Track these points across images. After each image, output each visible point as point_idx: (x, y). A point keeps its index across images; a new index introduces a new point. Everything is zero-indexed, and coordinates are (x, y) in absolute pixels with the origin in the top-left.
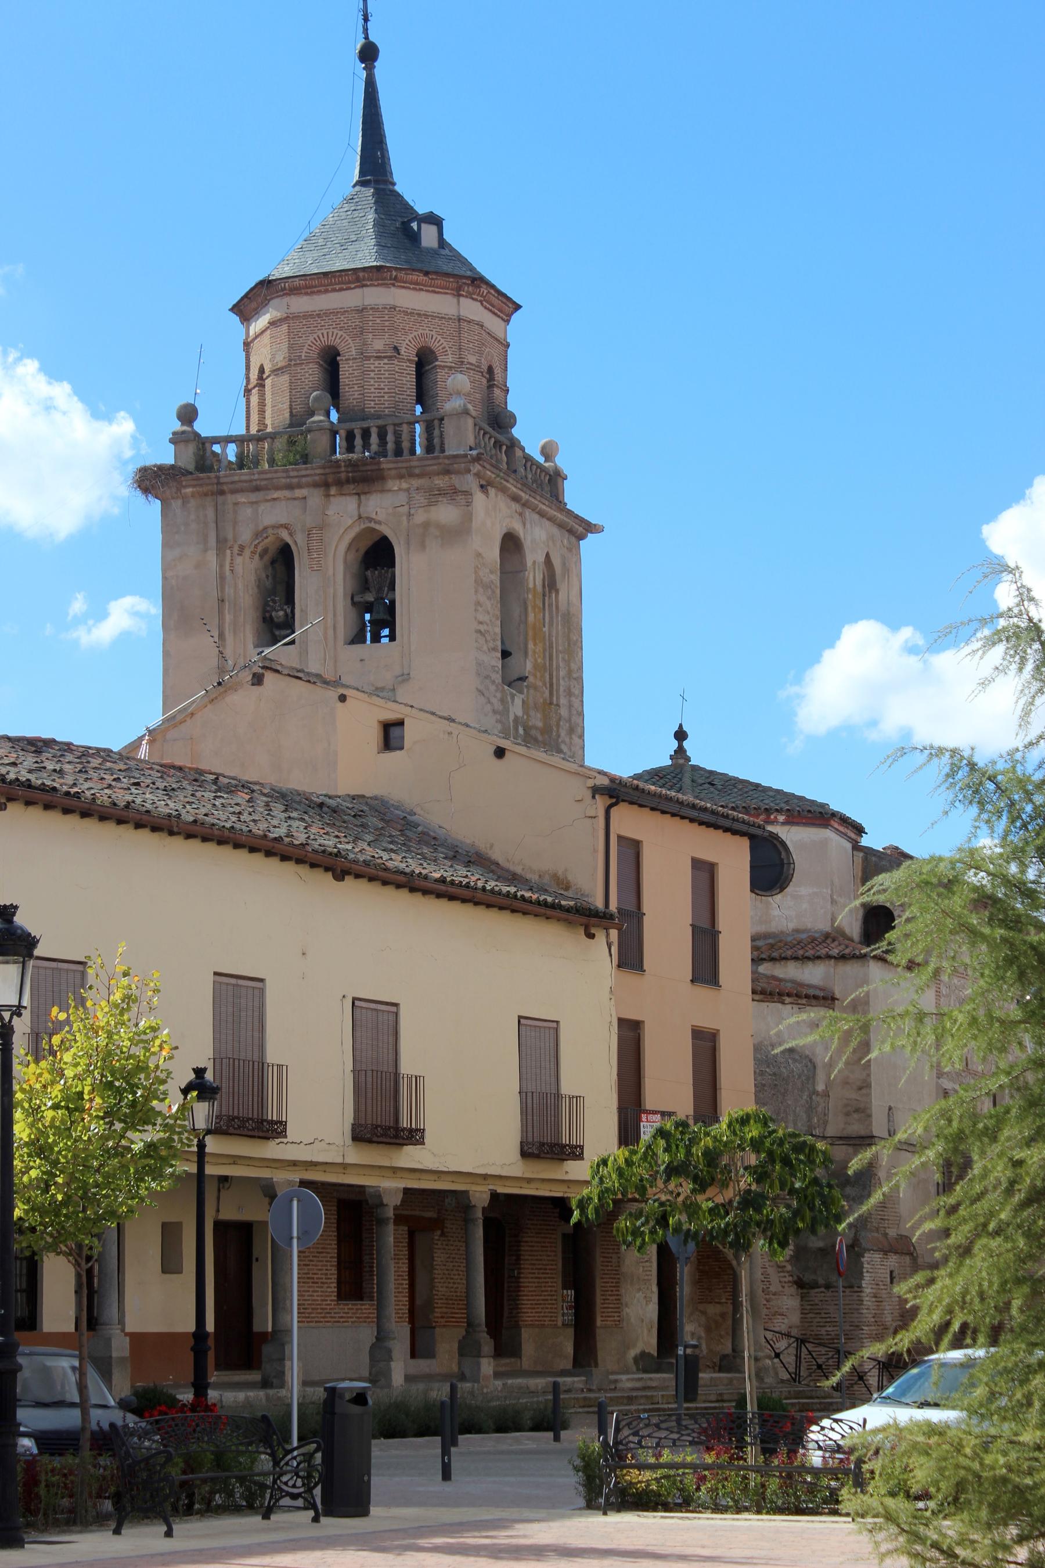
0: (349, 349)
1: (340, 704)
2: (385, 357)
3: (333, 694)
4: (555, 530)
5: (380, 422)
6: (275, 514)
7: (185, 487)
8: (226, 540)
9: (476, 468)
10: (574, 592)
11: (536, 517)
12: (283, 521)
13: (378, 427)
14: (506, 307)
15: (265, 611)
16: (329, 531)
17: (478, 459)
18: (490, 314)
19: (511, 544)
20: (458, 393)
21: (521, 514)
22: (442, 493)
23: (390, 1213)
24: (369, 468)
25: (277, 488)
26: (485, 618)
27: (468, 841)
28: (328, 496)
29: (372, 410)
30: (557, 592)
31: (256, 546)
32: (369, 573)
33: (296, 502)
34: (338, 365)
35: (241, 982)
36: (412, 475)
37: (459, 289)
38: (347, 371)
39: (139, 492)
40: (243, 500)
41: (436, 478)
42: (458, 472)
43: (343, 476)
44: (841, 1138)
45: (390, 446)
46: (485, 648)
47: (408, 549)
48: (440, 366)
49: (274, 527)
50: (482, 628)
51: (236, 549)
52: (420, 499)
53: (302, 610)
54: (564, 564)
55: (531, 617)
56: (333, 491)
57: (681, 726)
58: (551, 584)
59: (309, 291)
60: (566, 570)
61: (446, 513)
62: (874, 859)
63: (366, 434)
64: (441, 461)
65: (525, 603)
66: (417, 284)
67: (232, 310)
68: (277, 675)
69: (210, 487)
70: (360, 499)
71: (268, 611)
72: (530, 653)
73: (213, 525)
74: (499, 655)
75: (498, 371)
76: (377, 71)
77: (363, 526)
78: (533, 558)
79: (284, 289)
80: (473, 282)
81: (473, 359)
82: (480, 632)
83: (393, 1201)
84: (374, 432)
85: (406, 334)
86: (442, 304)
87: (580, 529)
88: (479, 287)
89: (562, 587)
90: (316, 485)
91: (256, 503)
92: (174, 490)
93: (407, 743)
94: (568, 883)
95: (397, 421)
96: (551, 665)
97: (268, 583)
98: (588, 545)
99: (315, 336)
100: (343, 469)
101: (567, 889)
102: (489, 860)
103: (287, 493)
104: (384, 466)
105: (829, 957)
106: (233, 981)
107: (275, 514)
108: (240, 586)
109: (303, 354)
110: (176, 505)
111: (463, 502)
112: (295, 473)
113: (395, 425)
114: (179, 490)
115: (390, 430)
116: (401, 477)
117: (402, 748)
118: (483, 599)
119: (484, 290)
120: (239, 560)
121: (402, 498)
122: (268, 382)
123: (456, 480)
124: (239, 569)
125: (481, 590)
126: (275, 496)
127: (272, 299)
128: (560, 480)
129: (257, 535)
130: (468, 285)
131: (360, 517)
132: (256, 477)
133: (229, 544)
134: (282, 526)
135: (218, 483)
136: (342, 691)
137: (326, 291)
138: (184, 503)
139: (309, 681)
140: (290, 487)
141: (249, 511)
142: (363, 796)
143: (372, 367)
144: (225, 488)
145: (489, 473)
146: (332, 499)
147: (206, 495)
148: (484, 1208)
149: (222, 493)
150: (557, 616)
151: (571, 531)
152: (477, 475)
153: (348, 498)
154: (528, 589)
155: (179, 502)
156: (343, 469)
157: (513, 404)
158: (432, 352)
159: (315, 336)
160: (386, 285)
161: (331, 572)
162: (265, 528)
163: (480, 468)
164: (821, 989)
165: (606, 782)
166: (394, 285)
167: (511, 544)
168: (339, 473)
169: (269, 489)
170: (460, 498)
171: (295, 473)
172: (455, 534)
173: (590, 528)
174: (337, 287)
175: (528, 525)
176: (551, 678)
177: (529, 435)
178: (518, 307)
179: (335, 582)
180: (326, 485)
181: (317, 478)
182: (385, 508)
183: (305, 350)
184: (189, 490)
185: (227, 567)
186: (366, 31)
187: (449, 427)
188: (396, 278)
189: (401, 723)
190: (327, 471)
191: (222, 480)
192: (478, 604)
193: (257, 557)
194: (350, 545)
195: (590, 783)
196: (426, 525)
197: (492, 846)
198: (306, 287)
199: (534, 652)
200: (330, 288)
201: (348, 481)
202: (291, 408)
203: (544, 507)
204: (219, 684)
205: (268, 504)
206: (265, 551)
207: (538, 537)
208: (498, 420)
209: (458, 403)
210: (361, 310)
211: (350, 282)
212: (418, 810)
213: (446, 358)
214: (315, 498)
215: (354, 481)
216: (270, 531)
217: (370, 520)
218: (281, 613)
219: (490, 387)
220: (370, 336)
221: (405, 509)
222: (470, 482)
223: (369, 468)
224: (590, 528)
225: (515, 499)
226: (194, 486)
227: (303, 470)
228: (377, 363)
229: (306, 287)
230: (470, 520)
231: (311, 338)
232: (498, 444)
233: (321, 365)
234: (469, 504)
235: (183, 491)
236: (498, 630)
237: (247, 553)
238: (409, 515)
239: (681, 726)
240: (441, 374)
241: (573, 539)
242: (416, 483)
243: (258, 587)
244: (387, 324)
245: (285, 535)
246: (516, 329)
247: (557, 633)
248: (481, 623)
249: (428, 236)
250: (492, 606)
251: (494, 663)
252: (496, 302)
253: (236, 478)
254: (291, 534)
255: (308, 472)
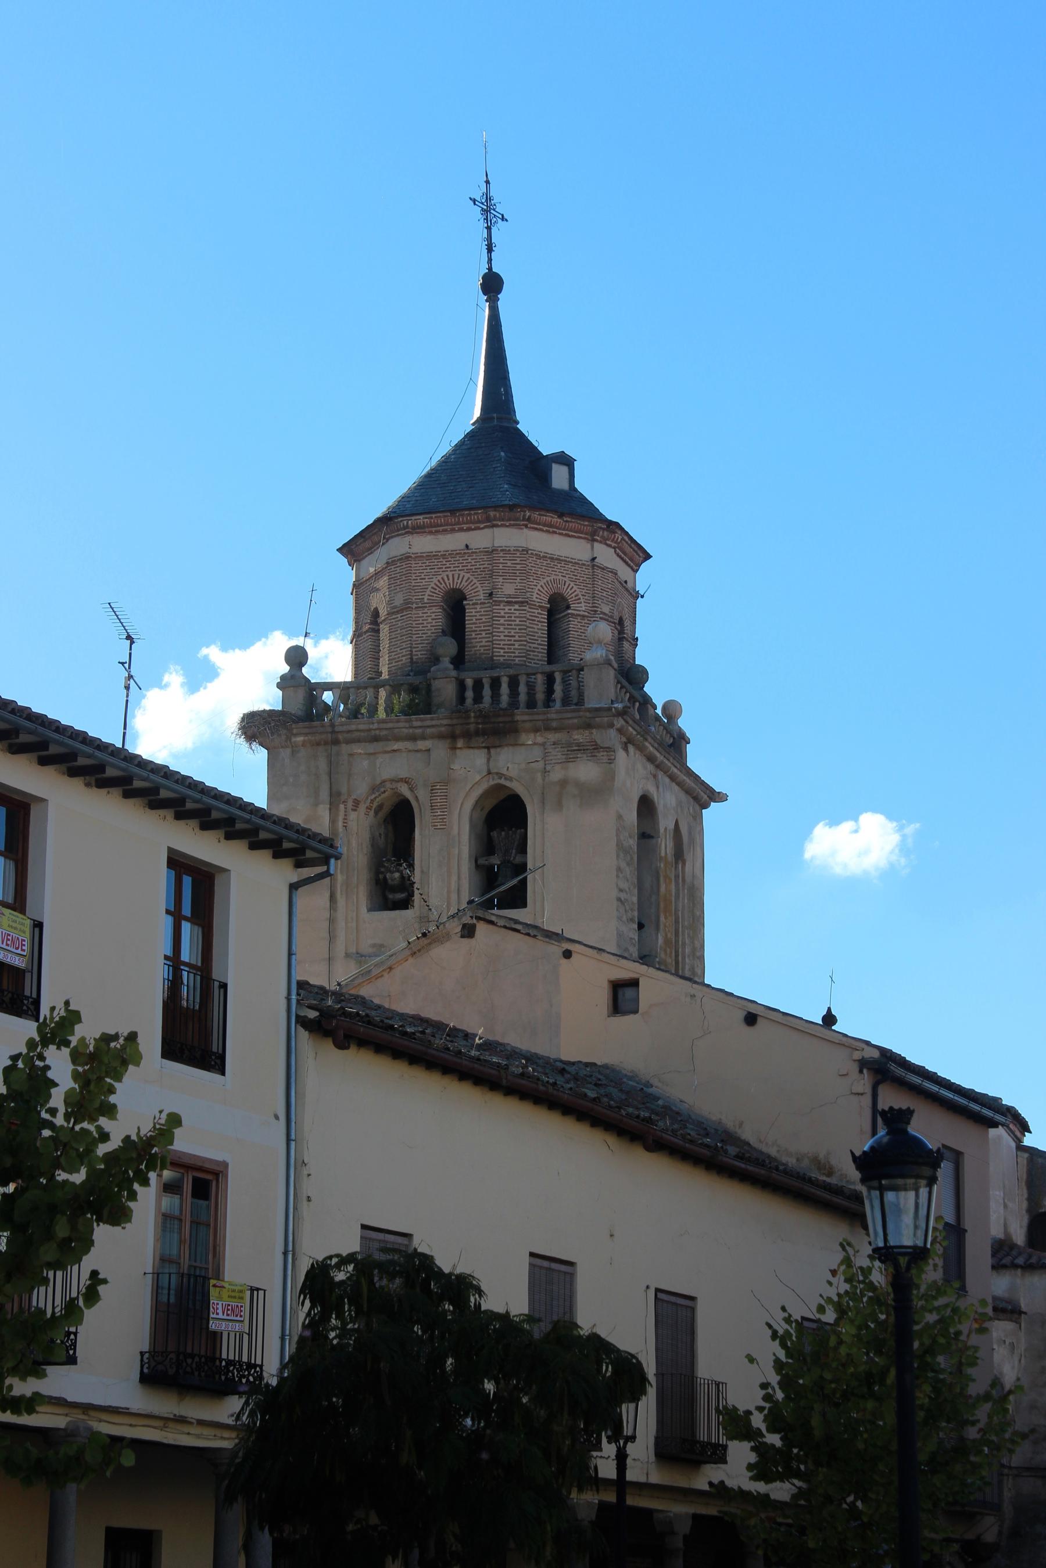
0: (476, 592)
1: (564, 961)
2: (516, 603)
3: (555, 949)
4: (683, 796)
5: (512, 672)
6: (396, 766)
7: (296, 735)
8: (339, 794)
9: (619, 722)
10: (698, 864)
11: (667, 780)
12: (403, 775)
13: (509, 677)
14: (636, 555)
15: (377, 872)
16: (454, 784)
17: (622, 713)
18: (621, 562)
19: (646, 806)
20: (599, 642)
21: (655, 776)
22: (581, 748)
23: (679, 1543)
24: (501, 719)
25: (397, 739)
26: (624, 885)
27: (714, 1119)
28: (454, 748)
29: (502, 659)
30: (684, 864)
31: (372, 801)
32: (494, 834)
33: (419, 755)
34: (464, 609)
35: (554, 1266)
36: (548, 729)
37: (594, 533)
38: (474, 616)
39: (242, 740)
40: (360, 751)
41: (576, 732)
42: (599, 727)
43: (472, 727)
44: (1028, 1469)
45: (523, 697)
46: (624, 918)
47: (544, 808)
48: (573, 614)
49: (392, 781)
50: (623, 896)
51: (350, 804)
52: (556, 754)
53: (422, 872)
54: (690, 833)
55: (663, 889)
56: (460, 743)
57: (829, 1009)
58: (679, 854)
59: (434, 529)
60: (692, 841)
61: (586, 771)
62: (1040, 1160)
63: (495, 683)
64: (581, 713)
65: (658, 873)
66: (551, 526)
67: (340, 550)
68: (491, 927)
69: (324, 736)
70: (489, 753)
71: (382, 873)
72: (662, 927)
73: (325, 778)
74: (636, 926)
75: (627, 623)
76: (501, 304)
77: (492, 783)
78: (665, 823)
79: (405, 528)
80: (608, 527)
81: (606, 609)
82: (619, 899)
83: (684, 1528)
84: (486, 683)
85: (538, 579)
86: (573, 548)
87: (703, 795)
88: (615, 533)
89: (688, 857)
90: (441, 737)
91: (374, 754)
92: (284, 737)
93: (643, 1005)
94: (831, 1168)
95: (530, 671)
96: (677, 941)
97: (381, 842)
98: (711, 815)
99: (439, 578)
100: (472, 720)
101: (830, 1174)
102: (738, 1139)
103: (409, 745)
104: (518, 718)
105: (1016, 1266)
106: (546, 1264)
107: (396, 766)
108: (354, 843)
109: (426, 597)
110: (285, 753)
111: (605, 759)
112: (419, 724)
113: (528, 675)
114: (288, 739)
115: (523, 680)
116: (536, 730)
117: (636, 1012)
118: (623, 865)
119: (619, 536)
120: (353, 815)
121: (537, 752)
122: (384, 629)
123: (596, 735)
124: (353, 825)
125: (622, 855)
126: (395, 747)
127: (392, 537)
128: (684, 743)
129: (374, 789)
130: (604, 529)
131: (489, 773)
132: (376, 726)
133: (343, 798)
134: (401, 780)
135: (333, 732)
136: (567, 946)
137: (453, 531)
138: (293, 753)
139: (528, 934)
140: (413, 738)
141: (366, 763)
142: (595, 1064)
143: (502, 612)
144: (340, 737)
145: (630, 728)
146: (458, 751)
147: (318, 744)
148: (685, 1536)
149: (336, 742)
150: (683, 890)
151: (696, 799)
152: (620, 731)
153: (476, 751)
154: (661, 857)
155: (288, 751)
156: (472, 720)
157: (642, 657)
158: (564, 599)
159: (439, 578)
160: (518, 526)
161: (455, 831)
162: (384, 781)
163: (623, 723)
164: (1007, 1302)
165: (876, 1054)
166: (526, 526)
167: (646, 806)
168: (468, 724)
169: (388, 740)
170: (601, 754)
171: (419, 724)
172: (594, 794)
173: (716, 797)
174: (465, 526)
175: (661, 789)
176: (677, 956)
177: (658, 691)
178: (648, 556)
179: (459, 842)
180: (453, 737)
181: (443, 729)
182: (517, 764)
183: (428, 592)
184: (300, 739)
185: (340, 824)
186: (490, 260)
187: (589, 678)
188: (529, 519)
189: (634, 983)
190: (455, 721)
191: (337, 729)
192: (619, 869)
193: (372, 813)
194: (477, 802)
195: (857, 1055)
196: (563, 783)
197: (741, 1124)
198: (431, 526)
199: (665, 926)
200: (456, 527)
201: (477, 733)
202: (411, 654)
203: (676, 770)
204: (424, 935)
205: (387, 756)
206: (380, 807)
207: (668, 800)
208: (633, 677)
209: (599, 654)
210: (492, 552)
211: (479, 522)
212: (655, 1082)
213: (580, 607)
214: (440, 750)
215: (484, 733)
216: (388, 785)
217: (500, 775)
218: (397, 875)
219: (621, 639)
220: (501, 579)
221: (541, 764)
222: (611, 738)
223: (501, 719)
224: (716, 797)
225: (651, 759)
226: (306, 734)
227: (428, 720)
228: (507, 608)
229: (431, 526)
230: (613, 778)
231: (435, 580)
232: (632, 699)
233: (444, 610)
234: (611, 761)
235: (293, 739)
236: (635, 899)
237: (362, 808)
238: (545, 771)
239: (829, 1009)
240: (574, 624)
241: (698, 807)
242: (552, 737)
243: (372, 845)
244: (518, 567)
245: (405, 790)
246: (644, 578)
247: (683, 906)
248: (621, 890)
249: (558, 478)
250: (630, 872)
251: (631, 935)
252: (628, 550)
253: (353, 727)
254: (411, 790)
255: (434, 723)
